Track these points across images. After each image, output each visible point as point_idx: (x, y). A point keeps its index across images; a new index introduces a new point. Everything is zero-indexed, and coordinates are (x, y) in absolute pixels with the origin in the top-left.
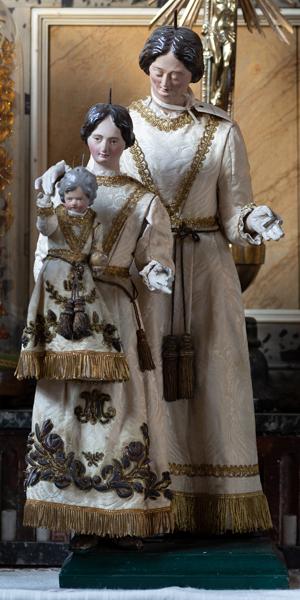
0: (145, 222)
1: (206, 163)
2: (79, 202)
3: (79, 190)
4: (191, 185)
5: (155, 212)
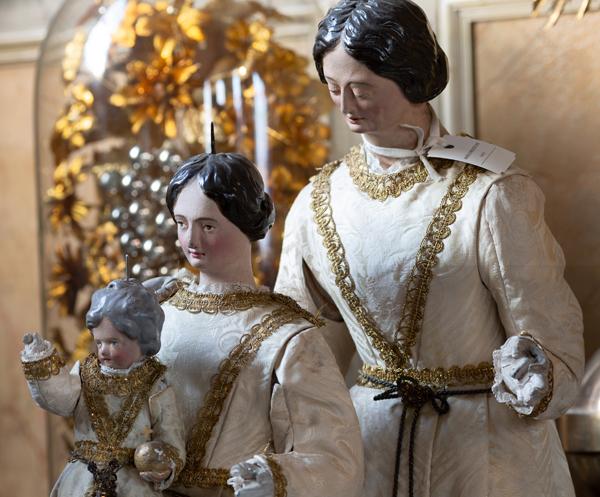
0: (274, 379)
1: (444, 257)
2: (112, 347)
3: (106, 322)
4: (422, 302)
5: (297, 357)
